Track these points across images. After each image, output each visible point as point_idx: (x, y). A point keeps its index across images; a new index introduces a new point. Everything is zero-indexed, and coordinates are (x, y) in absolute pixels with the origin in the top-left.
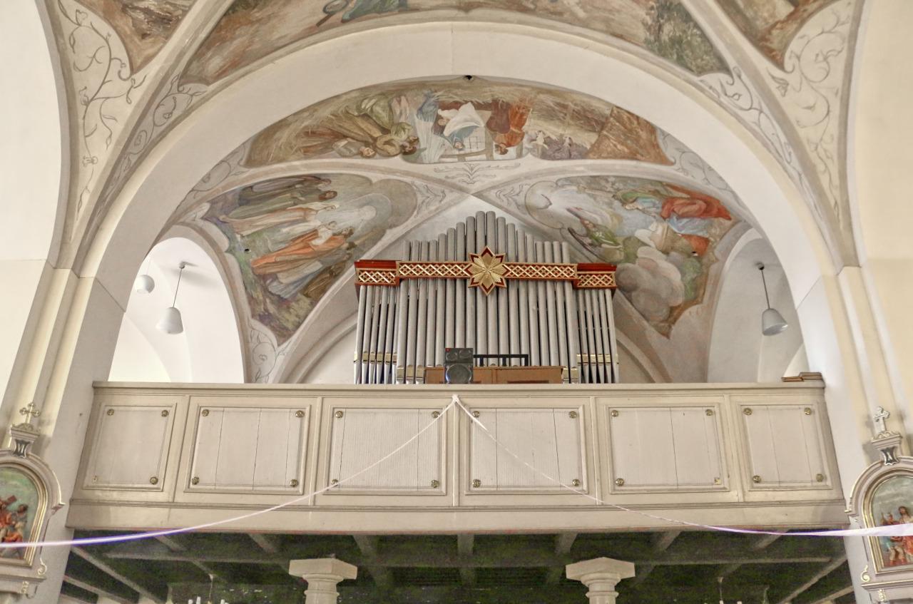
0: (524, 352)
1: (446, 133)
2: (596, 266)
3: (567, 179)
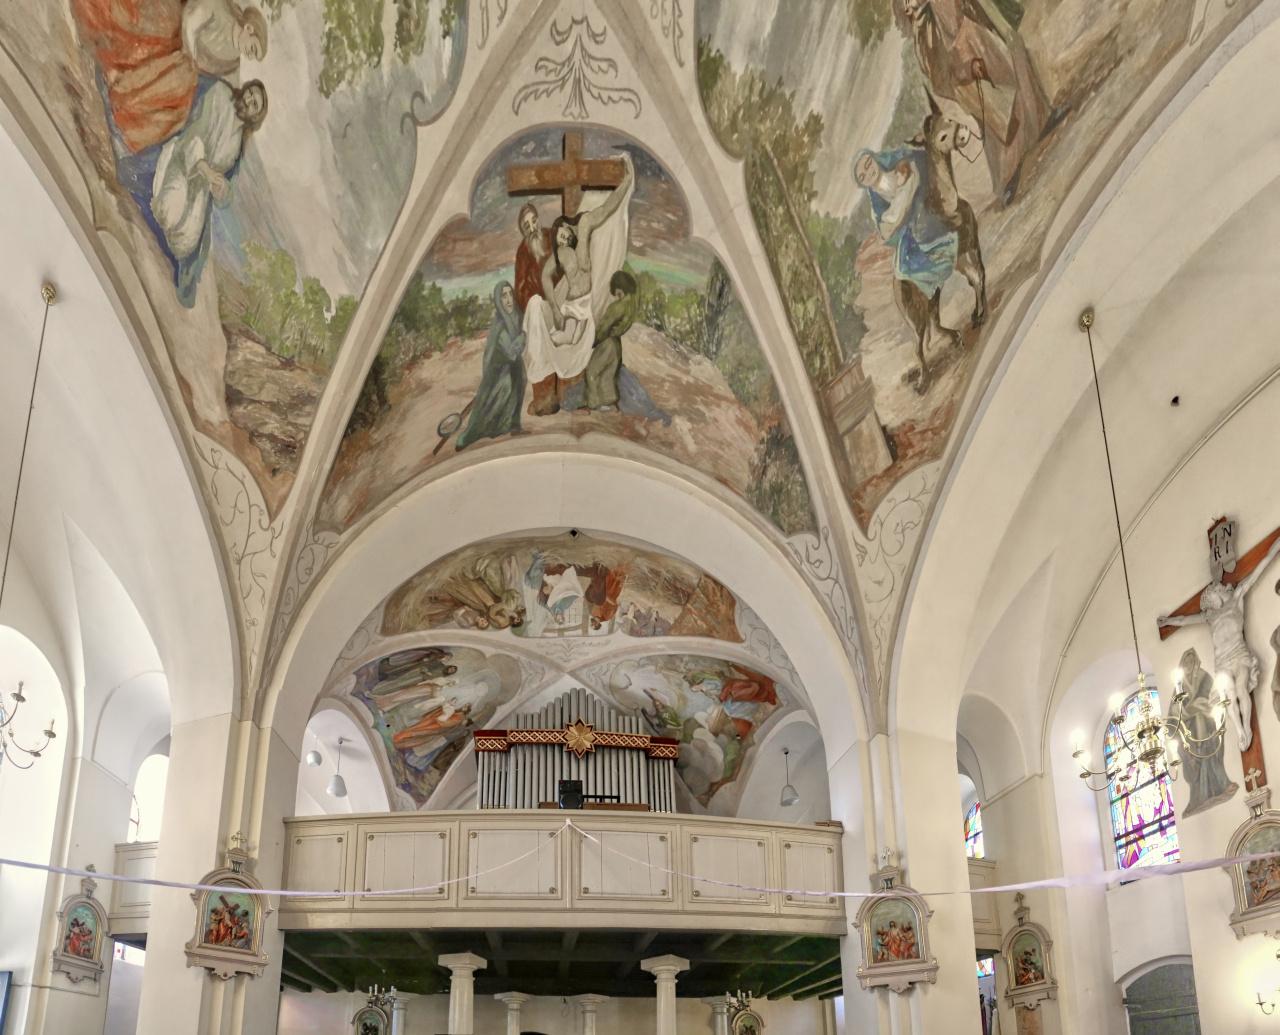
0: (615, 794)
1: (550, 603)
2: (661, 739)
3: (649, 658)
